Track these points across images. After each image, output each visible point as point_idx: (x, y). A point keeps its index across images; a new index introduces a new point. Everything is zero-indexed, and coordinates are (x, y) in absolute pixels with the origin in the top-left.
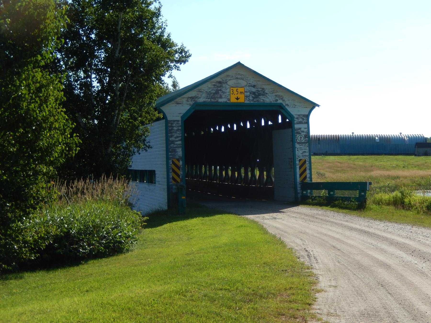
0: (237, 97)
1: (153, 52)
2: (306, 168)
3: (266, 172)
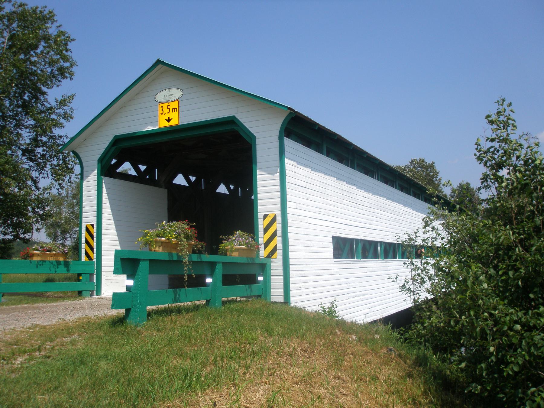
0: (169, 118)
1: (499, 226)
2: (276, 231)
3: (147, 307)
